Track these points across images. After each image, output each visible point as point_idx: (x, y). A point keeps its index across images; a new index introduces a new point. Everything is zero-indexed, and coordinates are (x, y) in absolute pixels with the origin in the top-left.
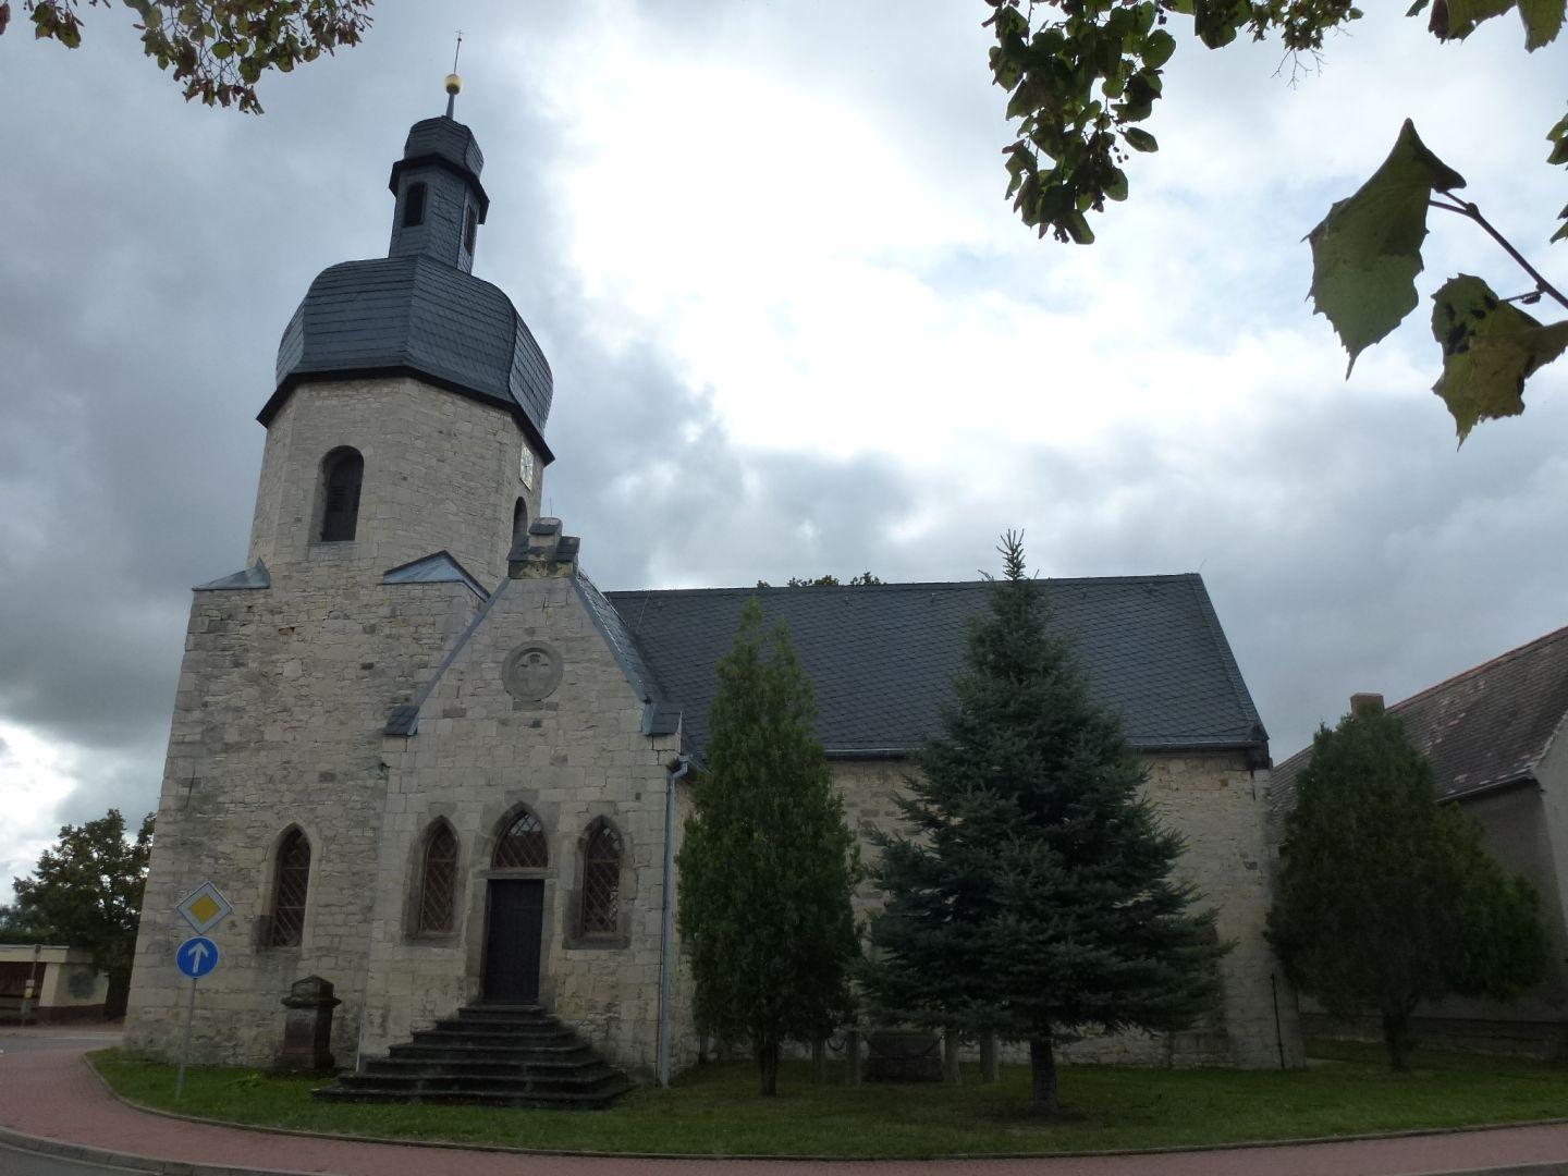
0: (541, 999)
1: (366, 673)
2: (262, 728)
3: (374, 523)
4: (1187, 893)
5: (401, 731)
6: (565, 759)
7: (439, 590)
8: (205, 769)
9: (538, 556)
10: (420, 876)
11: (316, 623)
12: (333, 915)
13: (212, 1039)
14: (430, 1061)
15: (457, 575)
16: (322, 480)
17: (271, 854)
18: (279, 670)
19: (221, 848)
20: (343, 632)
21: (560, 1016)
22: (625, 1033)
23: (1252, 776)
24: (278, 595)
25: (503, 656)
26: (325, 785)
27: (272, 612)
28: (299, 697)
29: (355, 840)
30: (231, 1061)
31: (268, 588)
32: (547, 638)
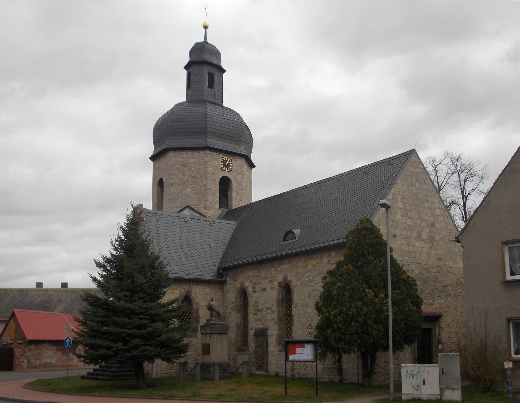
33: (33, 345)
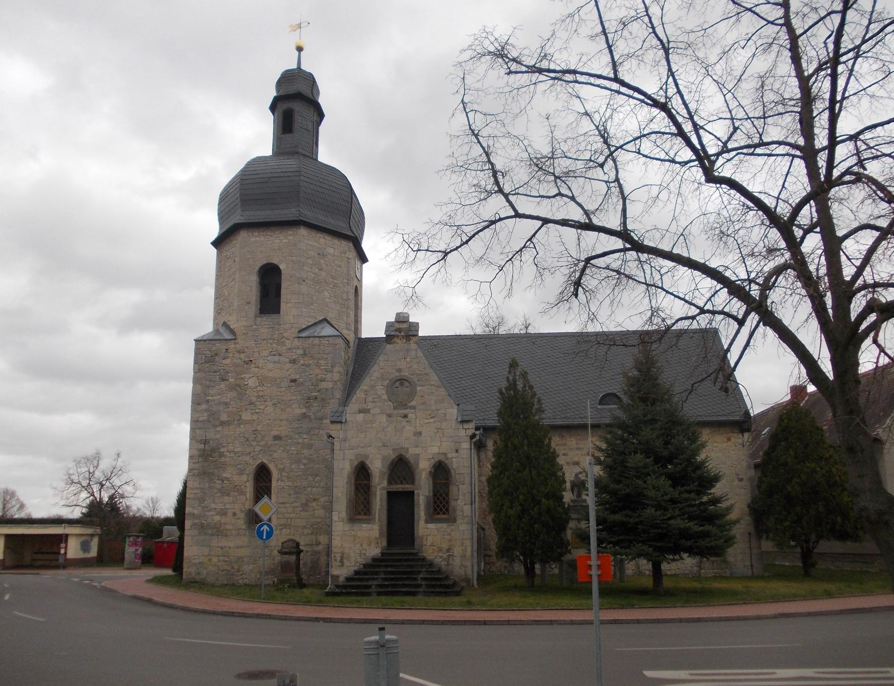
1: (293, 384)
2: (240, 413)
3: (289, 305)
4: (723, 498)
6: (420, 433)
8: (211, 435)
9: (400, 332)
10: (353, 491)
11: (264, 358)
12: (286, 508)
13: (229, 571)
14: (376, 577)
16: (258, 280)
17: (251, 478)
18: (246, 383)
19: (224, 475)
20: (279, 362)
21: (425, 555)
22: (457, 562)
23: (743, 435)
24: (241, 343)
25: (386, 383)
27: (239, 352)
28: (259, 397)
29: (295, 470)
30: (241, 582)
31: (235, 339)
32: (407, 374)
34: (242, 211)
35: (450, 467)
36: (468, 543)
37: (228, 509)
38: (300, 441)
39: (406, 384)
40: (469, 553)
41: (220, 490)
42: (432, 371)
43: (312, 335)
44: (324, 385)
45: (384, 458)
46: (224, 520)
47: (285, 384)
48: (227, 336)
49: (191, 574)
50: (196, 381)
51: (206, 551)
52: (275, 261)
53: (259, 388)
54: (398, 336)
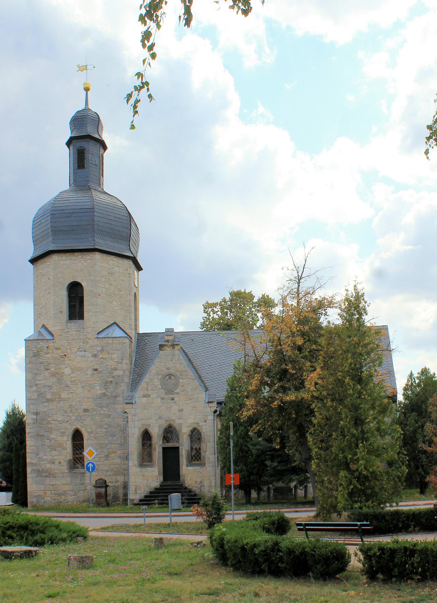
0: (181, 481)
1: (95, 372)
5: (130, 402)
6: (182, 410)
7: (118, 340)
8: (41, 408)
9: (168, 343)
15: (126, 336)
17: (70, 438)
18: (63, 371)
19: (51, 436)
25: (160, 376)
26: (85, 414)
27: (57, 349)
28: (71, 382)
29: (99, 432)
31: (53, 339)
33: (70, 460)
34: (53, 239)
35: (201, 432)
36: (213, 478)
37: (55, 459)
38: (102, 412)
39: (172, 377)
40: (213, 484)
41: (49, 447)
42: (189, 369)
43: (108, 336)
44: (116, 373)
45: (160, 426)
46: (53, 467)
47: (90, 372)
48: (49, 337)
49: (33, 503)
50: (28, 370)
51: (42, 487)
52: (79, 280)
53: (72, 375)
54: (167, 345)
